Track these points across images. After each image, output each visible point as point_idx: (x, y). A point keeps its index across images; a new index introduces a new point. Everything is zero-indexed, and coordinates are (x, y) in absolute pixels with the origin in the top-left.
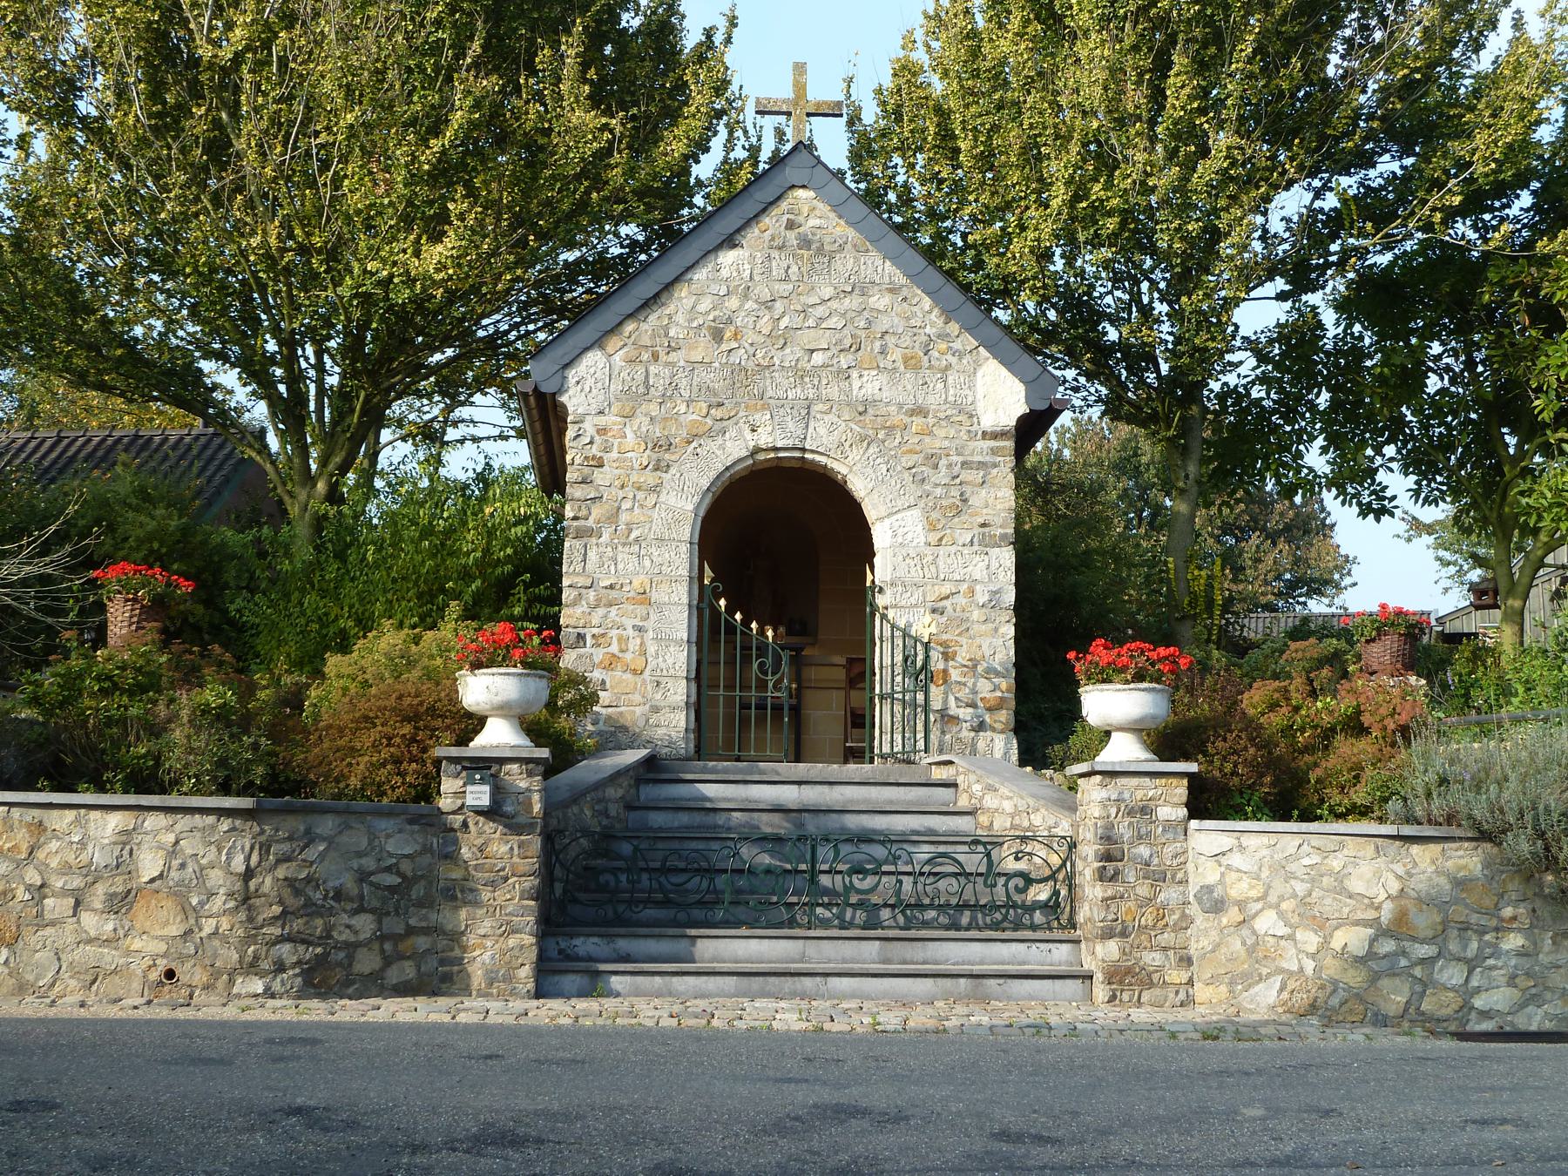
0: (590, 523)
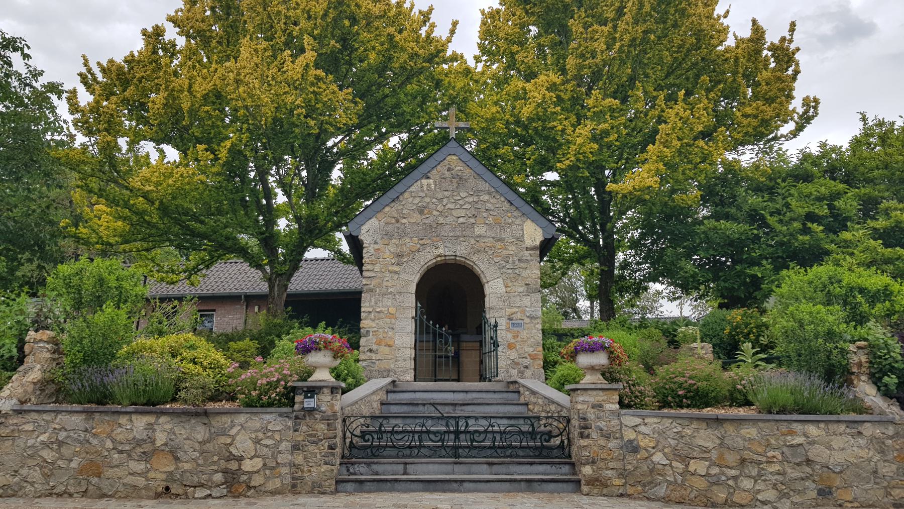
0: (371, 286)
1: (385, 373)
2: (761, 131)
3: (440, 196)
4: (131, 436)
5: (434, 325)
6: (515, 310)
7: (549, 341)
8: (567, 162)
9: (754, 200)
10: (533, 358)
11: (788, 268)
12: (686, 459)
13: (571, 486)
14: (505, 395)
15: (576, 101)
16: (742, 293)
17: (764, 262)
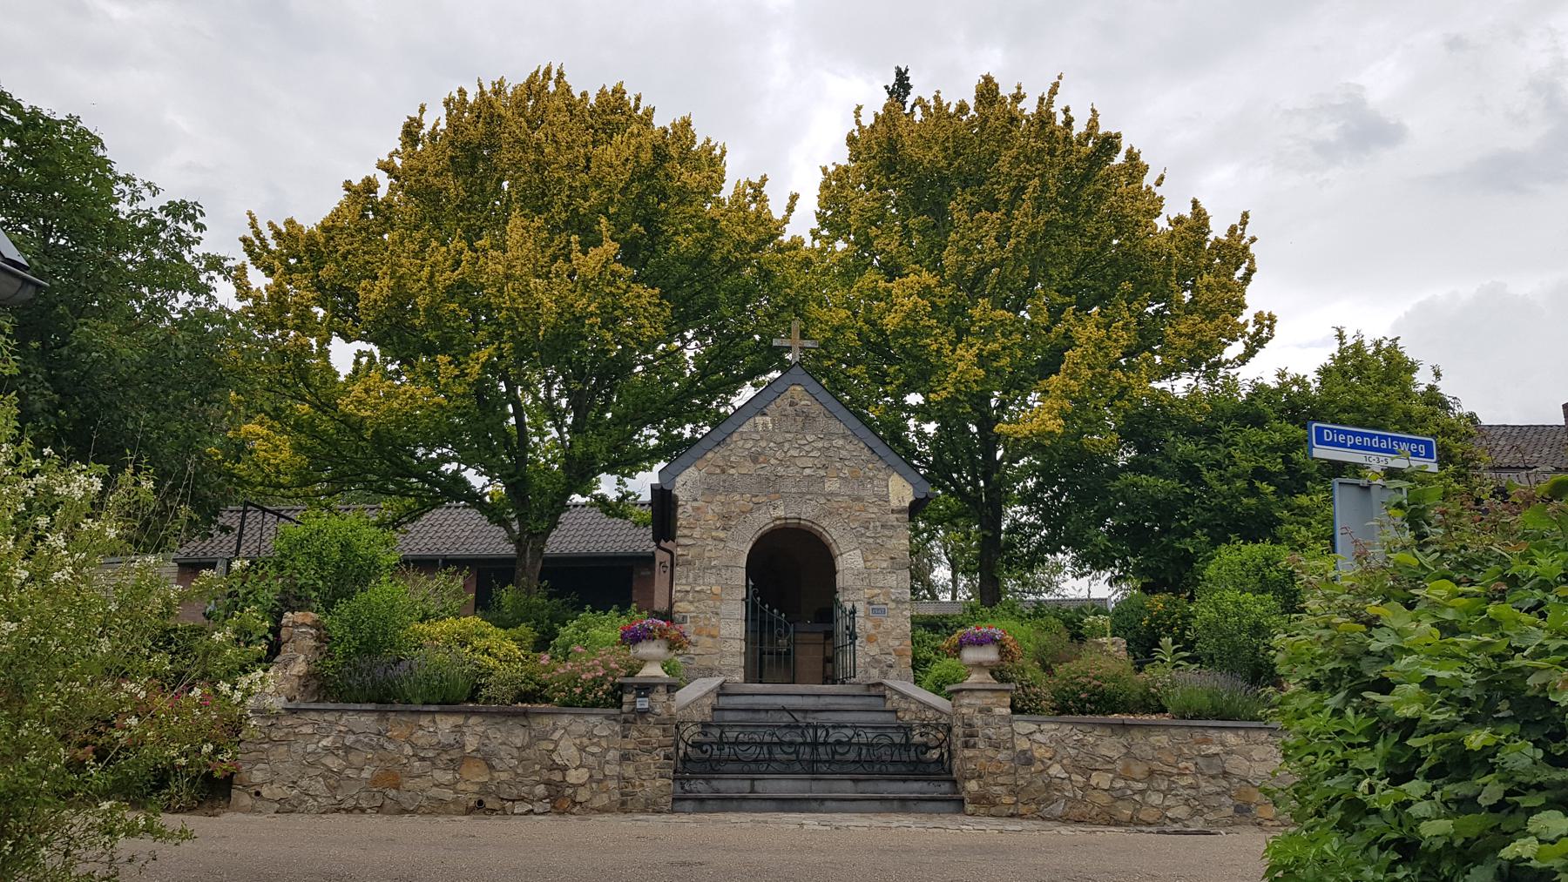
1: (709, 672)
2: (1201, 356)
3: (780, 439)
4: (434, 741)
5: (771, 610)
6: (877, 591)
7: (919, 632)
8: (944, 394)
9: (1185, 448)
10: (900, 655)
11: (1227, 541)
12: (1086, 771)
13: (952, 806)
14: (867, 700)
15: (957, 309)
16: (1168, 572)
17: (1198, 533)
